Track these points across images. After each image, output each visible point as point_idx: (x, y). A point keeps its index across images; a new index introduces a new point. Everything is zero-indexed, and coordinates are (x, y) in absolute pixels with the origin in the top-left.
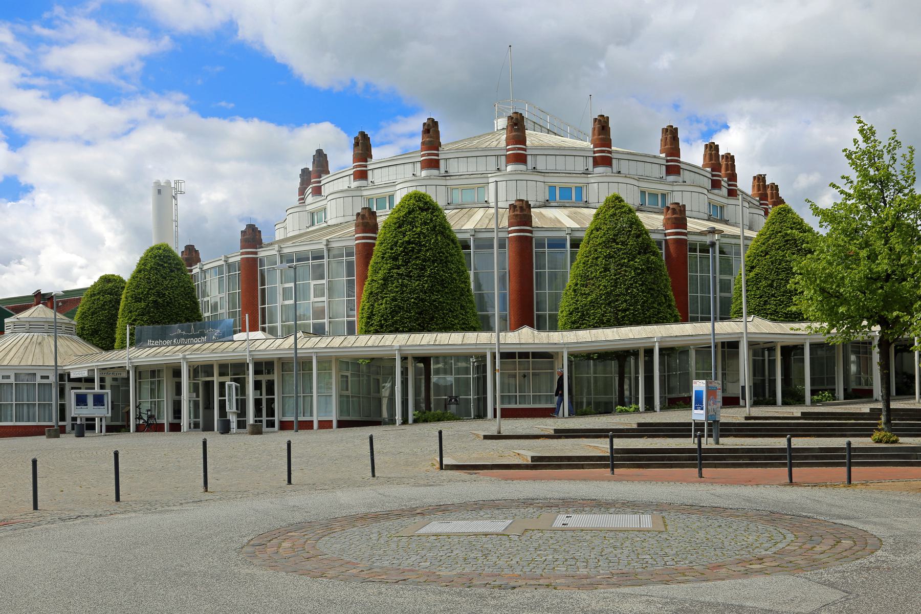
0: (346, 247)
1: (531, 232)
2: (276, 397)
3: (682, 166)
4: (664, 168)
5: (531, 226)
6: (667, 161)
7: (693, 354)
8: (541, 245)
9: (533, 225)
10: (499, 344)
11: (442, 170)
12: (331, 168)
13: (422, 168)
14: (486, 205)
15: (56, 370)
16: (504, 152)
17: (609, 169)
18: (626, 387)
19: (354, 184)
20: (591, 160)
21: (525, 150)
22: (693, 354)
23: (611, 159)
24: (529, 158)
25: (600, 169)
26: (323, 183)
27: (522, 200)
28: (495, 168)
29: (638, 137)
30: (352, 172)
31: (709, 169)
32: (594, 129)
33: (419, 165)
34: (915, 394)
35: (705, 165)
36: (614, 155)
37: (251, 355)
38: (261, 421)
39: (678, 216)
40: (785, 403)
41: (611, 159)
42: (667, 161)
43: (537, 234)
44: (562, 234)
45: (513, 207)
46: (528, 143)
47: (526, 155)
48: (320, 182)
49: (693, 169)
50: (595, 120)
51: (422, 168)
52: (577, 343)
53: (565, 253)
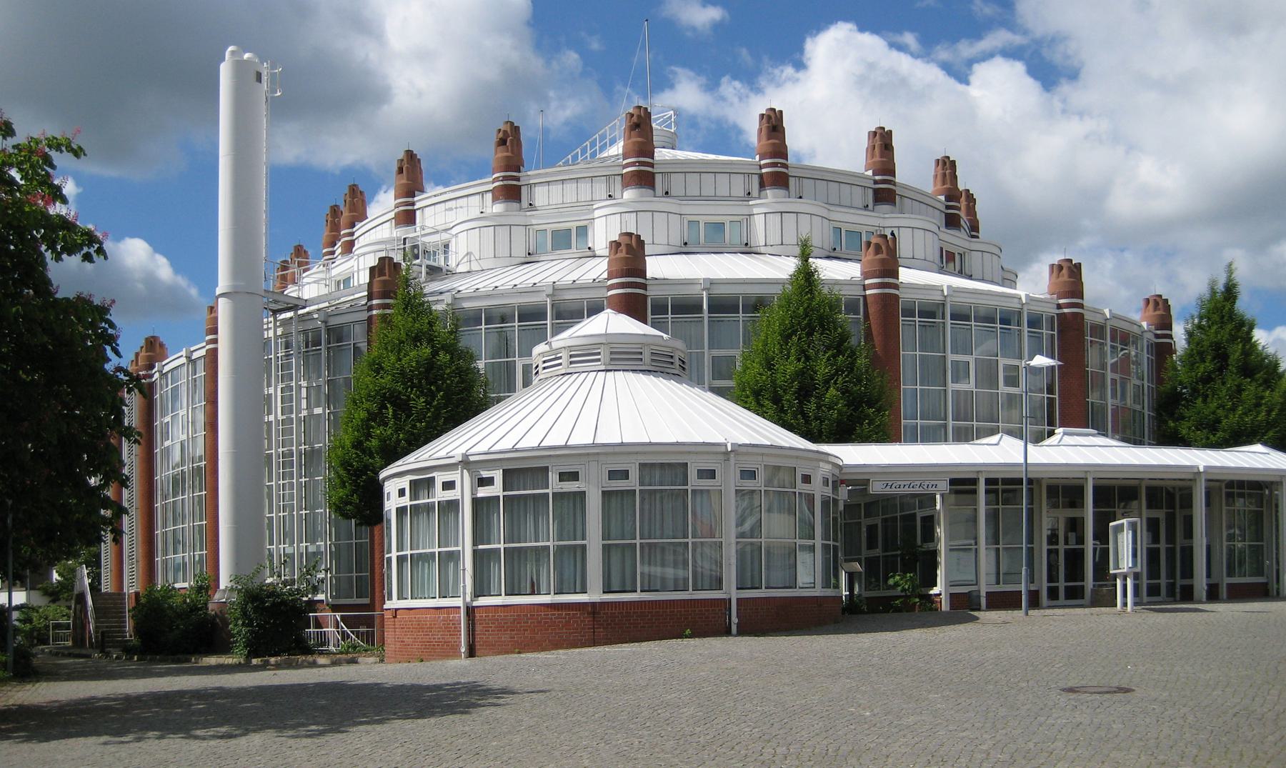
2: (1045, 547)
4: (870, 193)
6: (876, 182)
7: (982, 487)
9: (649, 275)
11: (525, 203)
14: (590, 253)
18: (613, 525)
19: (499, 208)
21: (652, 165)
24: (658, 178)
26: (356, 235)
27: (630, 235)
28: (605, 196)
31: (942, 198)
32: (760, 130)
34: (1094, 487)
36: (791, 172)
38: (1057, 551)
39: (886, 260)
40: (475, 552)
43: (652, 292)
45: (615, 245)
47: (653, 174)
48: (352, 234)
49: (919, 199)
50: (762, 116)
51: (495, 199)
53: (701, 320)
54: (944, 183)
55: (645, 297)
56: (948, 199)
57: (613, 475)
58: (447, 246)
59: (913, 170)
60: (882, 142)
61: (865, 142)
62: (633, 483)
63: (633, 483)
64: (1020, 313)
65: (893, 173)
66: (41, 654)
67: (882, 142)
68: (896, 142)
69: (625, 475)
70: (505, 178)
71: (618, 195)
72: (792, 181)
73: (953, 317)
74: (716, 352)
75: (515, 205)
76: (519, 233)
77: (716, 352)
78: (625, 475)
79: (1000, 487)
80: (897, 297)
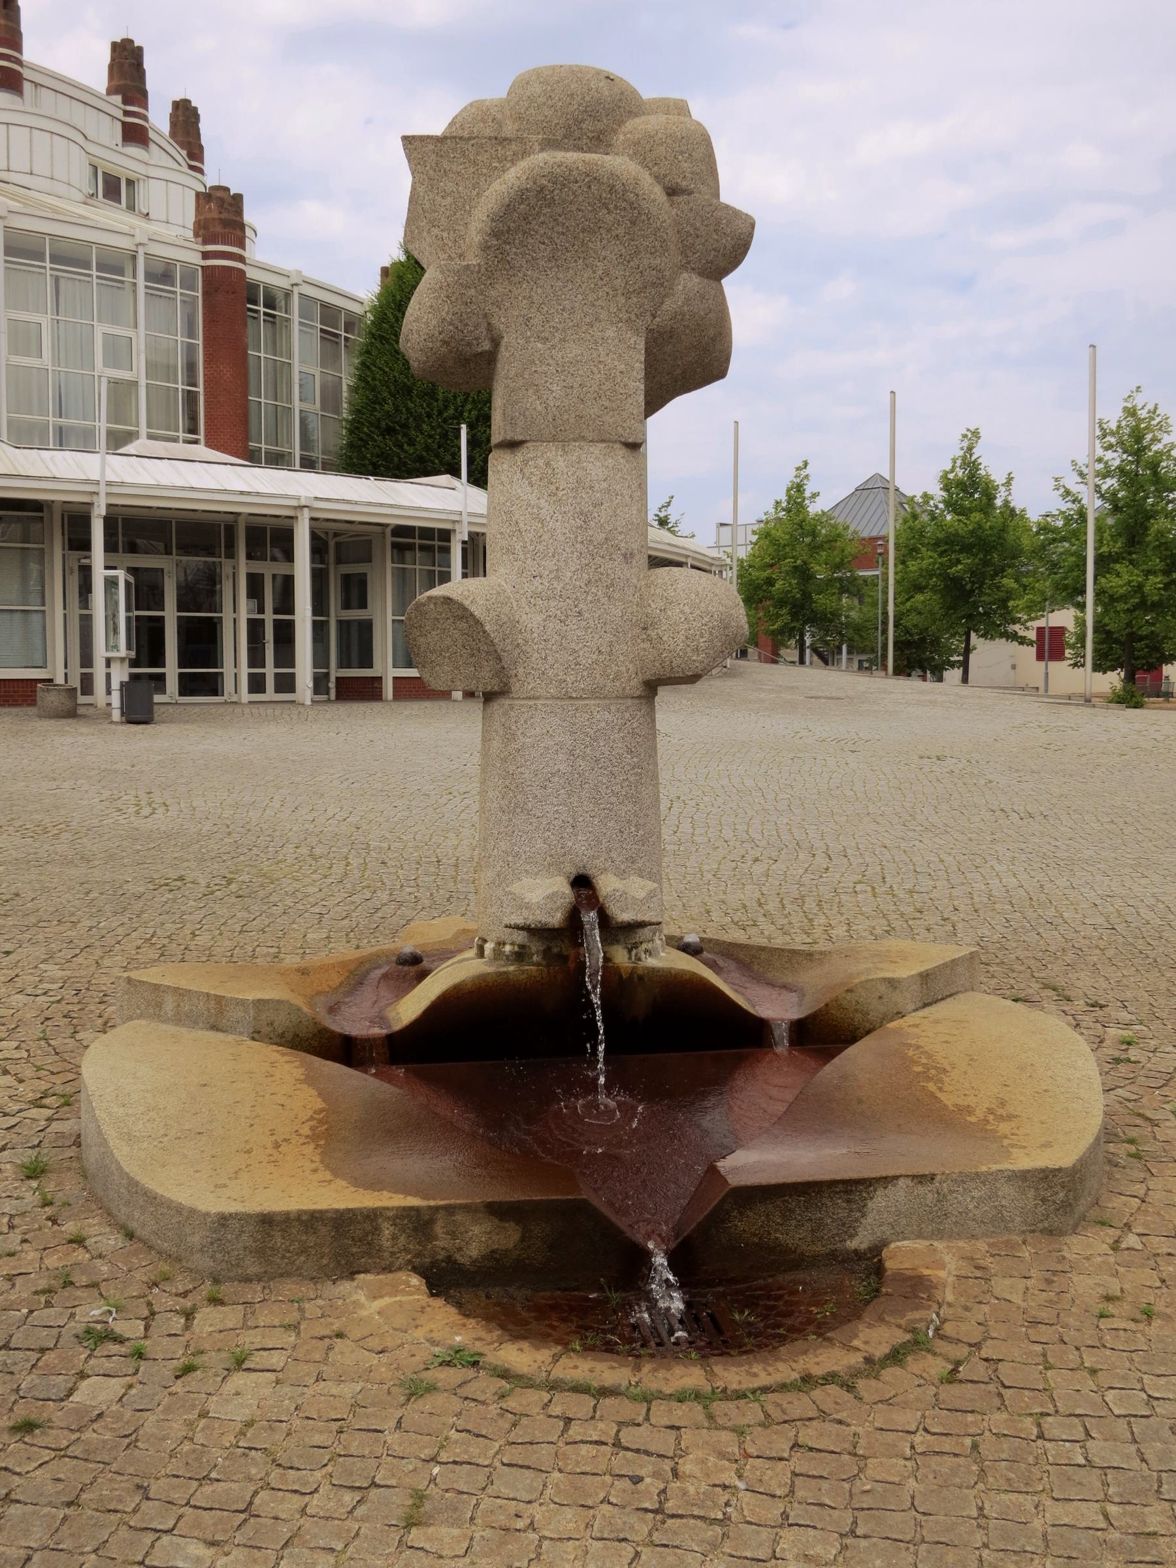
3: (26, 73)
72: (27, 86)
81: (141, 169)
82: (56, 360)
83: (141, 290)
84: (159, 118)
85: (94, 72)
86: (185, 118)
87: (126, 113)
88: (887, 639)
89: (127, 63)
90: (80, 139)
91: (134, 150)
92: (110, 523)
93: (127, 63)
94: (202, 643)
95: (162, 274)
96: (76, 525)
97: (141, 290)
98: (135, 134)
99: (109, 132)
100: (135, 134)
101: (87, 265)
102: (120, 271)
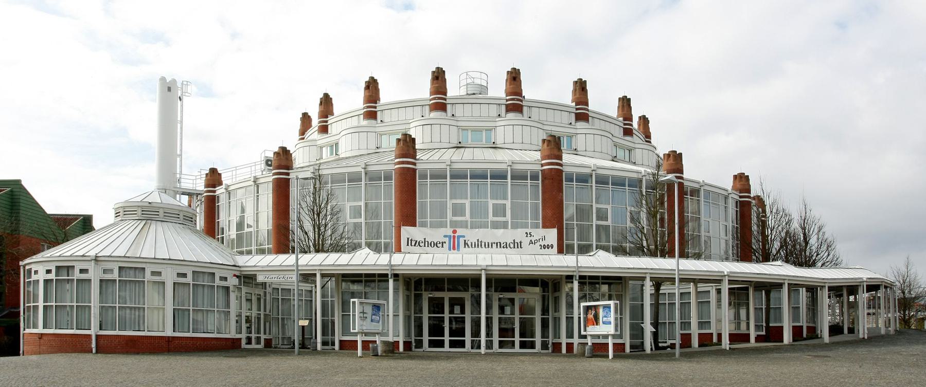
0: (385, 172)
1: (414, 164)
3: (590, 114)
4: (573, 115)
5: (415, 158)
8: (424, 177)
10: (679, 270)
11: (379, 121)
12: (335, 111)
13: (431, 110)
15: (298, 270)
16: (504, 102)
17: (444, 113)
19: (365, 123)
20: (504, 107)
22: (785, 289)
23: (522, 106)
25: (511, 115)
29: (547, 87)
30: (362, 112)
31: (621, 119)
33: (427, 108)
35: (618, 116)
37: (679, 274)
41: (522, 106)
42: (577, 109)
44: (504, 166)
46: (449, 94)
49: (605, 118)
51: (431, 110)
52: (522, 266)
54: (623, 110)
55: (415, 170)
56: (625, 119)
57: (179, 275)
58: (337, 144)
59: (603, 102)
60: (581, 87)
61: (571, 87)
62: (189, 279)
63: (189, 279)
64: (641, 181)
65: (587, 104)
66: (851, 310)
67: (581, 87)
68: (523, 77)
69: (184, 275)
70: (368, 107)
71: (427, 116)
72: (525, 109)
73: (452, 177)
74: (455, 201)
75: (373, 121)
76: (372, 136)
77: (455, 201)
78: (184, 275)
79: (587, 281)
80: (561, 171)
81: (632, 145)
82: (471, 217)
83: (594, 188)
84: (635, 124)
85: (613, 110)
86: (644, 120)
87: (625, 124)
88: (487, 313)
89: (625, 103)
90: (610, 136)
91: (628, 138)
92: (488, 281)
93: (625, 103)
94: (436, 329)
95: (519, 176)
96: (475, 281)
97: (594, 188)
98: (628, 132)
99: (619, 132)
100: (628, 132)
101: (624, 185)
102: (586, 181)
